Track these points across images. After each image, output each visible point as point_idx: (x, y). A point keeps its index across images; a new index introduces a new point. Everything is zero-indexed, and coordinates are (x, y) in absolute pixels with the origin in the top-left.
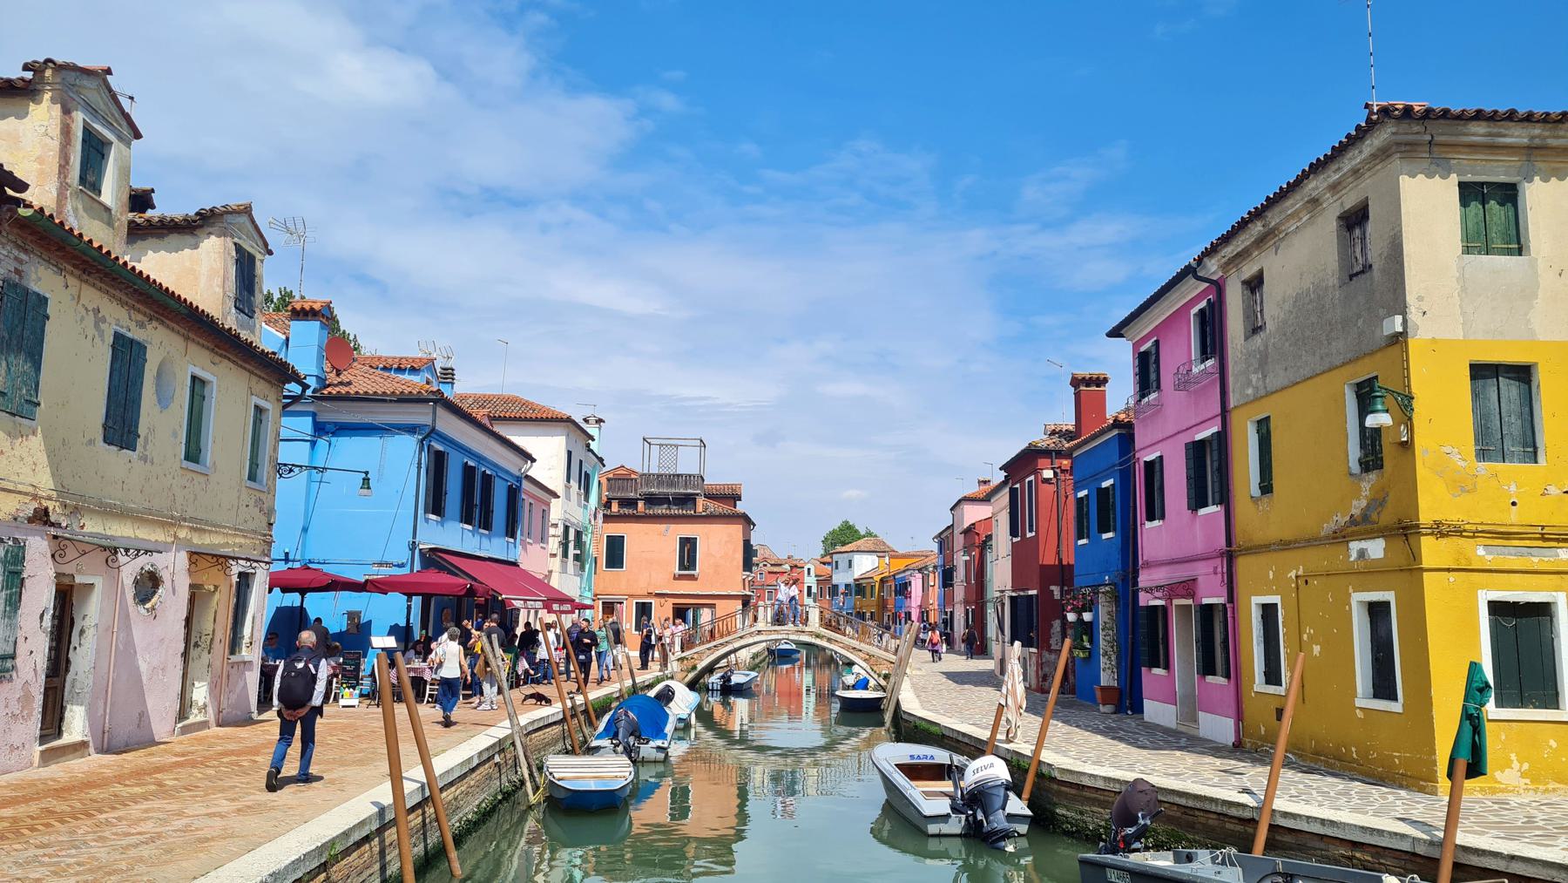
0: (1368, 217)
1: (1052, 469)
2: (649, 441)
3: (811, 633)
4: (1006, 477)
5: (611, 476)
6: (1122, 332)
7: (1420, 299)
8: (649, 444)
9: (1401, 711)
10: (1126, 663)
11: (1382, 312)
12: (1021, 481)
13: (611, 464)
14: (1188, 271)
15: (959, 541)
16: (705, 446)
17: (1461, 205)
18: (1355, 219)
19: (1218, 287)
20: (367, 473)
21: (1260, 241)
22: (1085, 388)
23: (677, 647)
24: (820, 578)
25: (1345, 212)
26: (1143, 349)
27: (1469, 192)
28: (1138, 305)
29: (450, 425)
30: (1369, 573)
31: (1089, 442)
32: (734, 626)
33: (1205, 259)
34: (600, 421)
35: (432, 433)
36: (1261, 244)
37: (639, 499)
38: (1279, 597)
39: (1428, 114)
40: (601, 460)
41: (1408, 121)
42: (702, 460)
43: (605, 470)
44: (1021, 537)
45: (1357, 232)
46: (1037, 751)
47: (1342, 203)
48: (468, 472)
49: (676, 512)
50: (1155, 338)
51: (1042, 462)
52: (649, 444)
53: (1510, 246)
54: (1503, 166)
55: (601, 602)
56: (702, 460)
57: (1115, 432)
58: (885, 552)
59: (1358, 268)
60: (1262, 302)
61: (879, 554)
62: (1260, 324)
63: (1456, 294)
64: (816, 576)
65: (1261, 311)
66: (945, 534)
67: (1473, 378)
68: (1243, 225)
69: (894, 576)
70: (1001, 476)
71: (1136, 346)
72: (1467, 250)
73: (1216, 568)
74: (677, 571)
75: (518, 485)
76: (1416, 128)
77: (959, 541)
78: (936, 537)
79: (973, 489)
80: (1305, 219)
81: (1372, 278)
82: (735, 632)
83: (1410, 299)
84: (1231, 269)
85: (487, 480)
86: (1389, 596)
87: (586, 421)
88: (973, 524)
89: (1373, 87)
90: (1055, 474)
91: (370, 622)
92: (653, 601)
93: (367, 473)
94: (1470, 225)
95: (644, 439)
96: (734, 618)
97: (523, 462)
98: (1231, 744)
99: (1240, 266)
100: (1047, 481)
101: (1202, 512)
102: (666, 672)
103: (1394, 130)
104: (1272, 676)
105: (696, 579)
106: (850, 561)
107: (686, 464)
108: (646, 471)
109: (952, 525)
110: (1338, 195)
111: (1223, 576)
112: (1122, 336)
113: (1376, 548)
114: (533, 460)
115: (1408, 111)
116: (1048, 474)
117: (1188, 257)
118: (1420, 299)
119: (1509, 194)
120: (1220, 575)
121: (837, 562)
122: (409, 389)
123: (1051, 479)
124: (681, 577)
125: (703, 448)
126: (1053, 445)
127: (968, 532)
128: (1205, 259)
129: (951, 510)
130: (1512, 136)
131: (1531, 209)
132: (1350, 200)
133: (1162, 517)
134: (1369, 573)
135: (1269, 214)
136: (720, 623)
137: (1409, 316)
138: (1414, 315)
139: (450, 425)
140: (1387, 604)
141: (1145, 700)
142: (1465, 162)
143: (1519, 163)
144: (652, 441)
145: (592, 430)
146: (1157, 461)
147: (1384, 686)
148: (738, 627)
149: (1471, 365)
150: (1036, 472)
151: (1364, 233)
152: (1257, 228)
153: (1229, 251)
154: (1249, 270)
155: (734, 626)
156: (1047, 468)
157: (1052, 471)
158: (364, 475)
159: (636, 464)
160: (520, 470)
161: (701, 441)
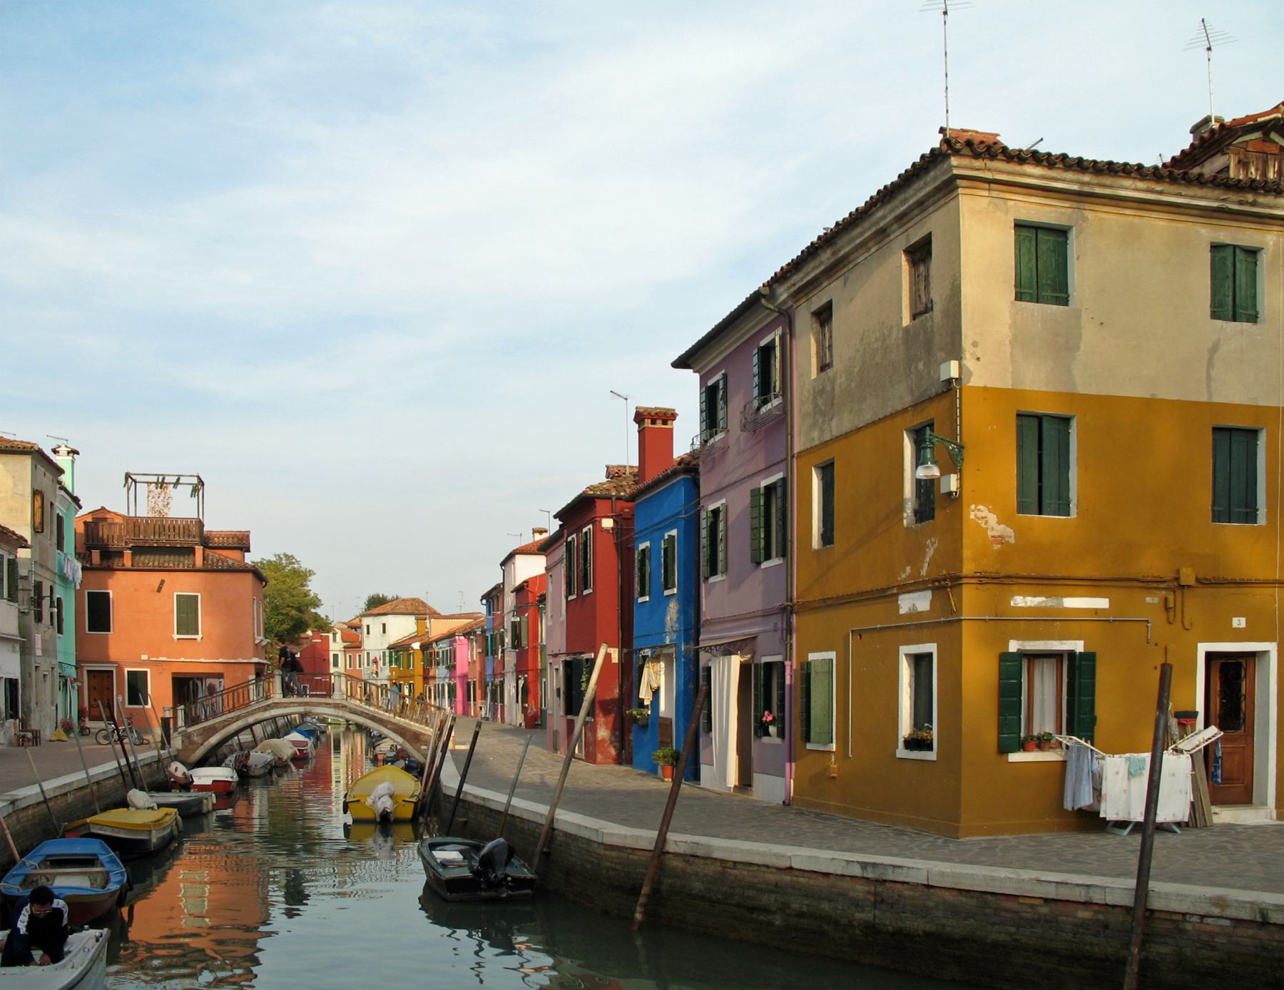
0: (931, 254)
2: (133, 477)
3: (336, 706)
4: (560, 526)
5: (89, 519)
6: (689, 362)
7: (975, 344)
8: (136, 482)
9: (935, 759)
10: (319, 704)
11: (941, 355)
12: (578, 530)
13: (89, 505)
15: (510, 600)
16: (203, 485)
18: (920, 253)
21: (830, 271)
22: (650, 426)
23: (181, 722)
25: (911, 246)
26: (710, 383)
30: (916, 627)
32: (246, 697)
36: (831, 274)
38: (834, 653)
40: (76, 500)
42: (200, 506)
43: (81, 513)
44: (577, 595)
45: (922, 268)
46: (1142, 890)
47: (908, 236)
50: (723, 372)
52: (136, 482)
53: (1059, 295)
54: (1056, 212)
55: (337, 697)
58: (425, 614)
59: (921, 308)
60: (831, 337)
62: (828, 361)
63: (1007, 342)
65: (830, 346)
70: (555, 526)
72: (1019, 297)
73: (776, 624)
77: (510, 600)
78: (483, 597)
79: (529, 539)
80: (873, 250)
81: (932, 318)
82: (248, 705)
83: (966, 343)
84: (801, 298)
86: (931, 648)
87: (55, 451)
88: (525, 582)
91: (555, 517)
92: (148, 670)
94: (1025, 274)
96: (246, 689)
98: (781, 803)
99: (810, 296)
101: (765, 565)
102: (171, 750)
107: (181, 507)
108: (132, 514)
109: (503, 583)
110: (905, 228)
111: (782, 633)
113: (917, 603)
120: (780, 632)
121: (368, 627)
127: (520, 590)
129: (502, 564)
131: (1078, 259)
132: (916, 235)
134: (916, 627)
135: (840, 243)
136: (231, 694)
137: (964, 362)
138: (969, 362)
140: (930, 655)
141: (702, 766)
142: (1021, 204)
143: (1069, 211)
144: (138, 478)
145: (62, 460)
148: (251, 699)
151: (928, 270)
152: (826, 257)
153: (800, 279)
154: (818, 301)
155: (246, 697)
159: (117, 504)
161: (198, 477)
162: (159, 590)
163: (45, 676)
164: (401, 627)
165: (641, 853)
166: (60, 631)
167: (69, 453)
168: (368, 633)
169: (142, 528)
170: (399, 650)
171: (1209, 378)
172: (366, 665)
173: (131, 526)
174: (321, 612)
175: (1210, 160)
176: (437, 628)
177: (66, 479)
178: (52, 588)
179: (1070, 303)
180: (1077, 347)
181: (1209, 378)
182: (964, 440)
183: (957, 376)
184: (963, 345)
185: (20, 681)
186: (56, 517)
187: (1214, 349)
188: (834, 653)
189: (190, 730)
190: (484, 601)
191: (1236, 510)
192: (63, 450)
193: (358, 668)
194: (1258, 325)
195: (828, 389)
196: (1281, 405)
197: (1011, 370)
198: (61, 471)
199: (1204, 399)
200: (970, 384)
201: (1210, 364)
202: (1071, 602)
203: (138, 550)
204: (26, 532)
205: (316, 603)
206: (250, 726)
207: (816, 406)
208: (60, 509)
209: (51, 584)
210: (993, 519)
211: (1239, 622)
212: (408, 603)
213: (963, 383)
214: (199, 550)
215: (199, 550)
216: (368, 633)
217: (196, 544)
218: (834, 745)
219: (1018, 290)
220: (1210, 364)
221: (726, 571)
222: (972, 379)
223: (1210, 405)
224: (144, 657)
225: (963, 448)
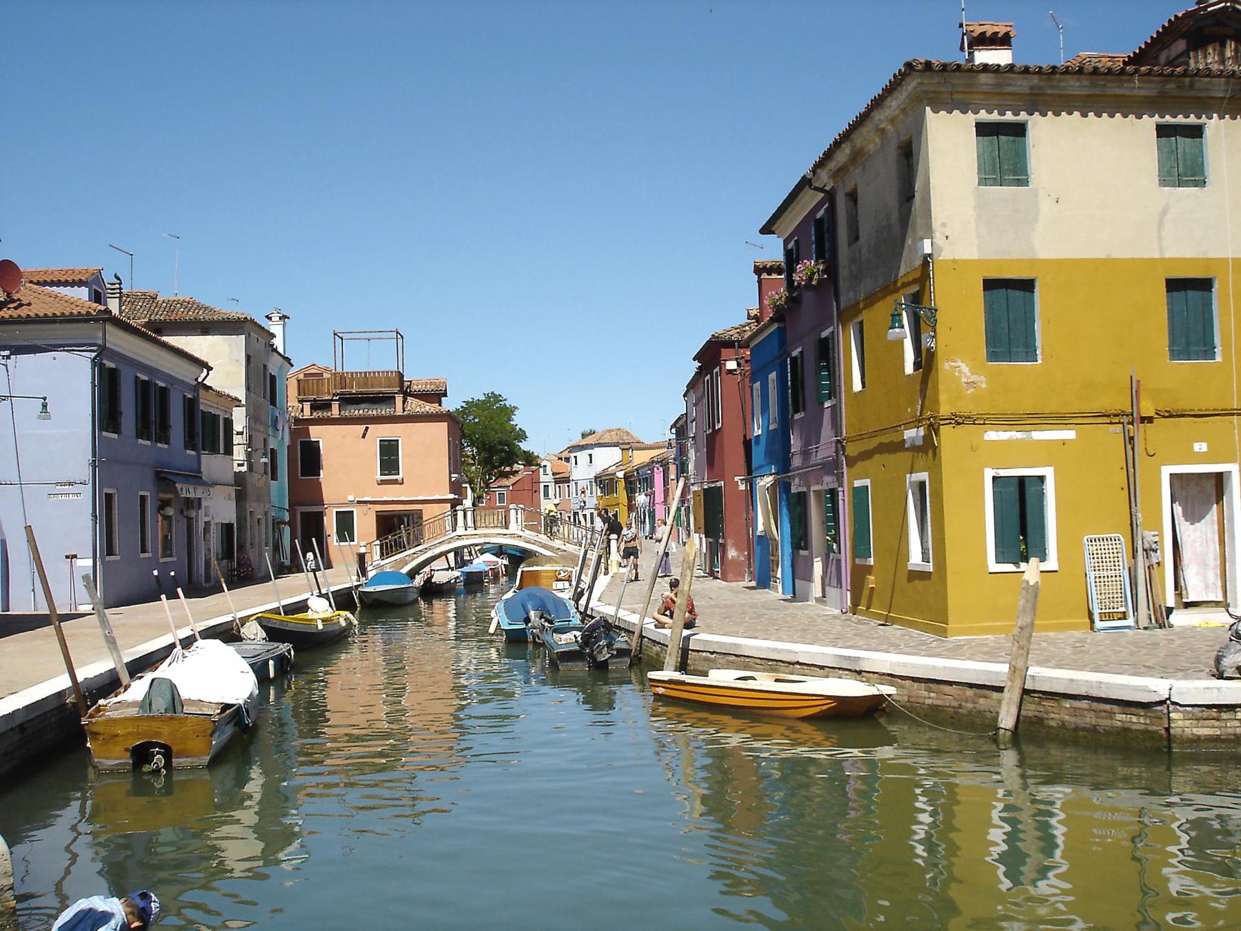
1: (736, 359)
3: (512, 536)
5: (301, 376)
6: (773, 229)
8: (342, 339)
14: (804, 183)
17: (5, 540)
19: (830, 196)
20: (45, 399)
22: (767, 277)
23: (377, 556)
24: (557, 476)
27: (983, 129)
28: (782, 201)
29: (118, 340)
31: (763, 330)
33: (818, 171)
34: (283, 318)
35: (103, 351)
37: (332, 400)
38: (869, 480)
39: (944, 67)
40: (288, 360)
41: (929, 73)
42: (400, 352)
43: (293, 370)
48: (144, 389)
49: (375, 413)
51: (725, 352)
56: (400, 352)
57: (775, 326)
61: (622, 447)
64: (554, 474)
66: (681, 423)
67: (985, 289)
68: (837, 144)
69: (637, 470)
71: (786, 242)
72: (983, 182)
74: (380, 477)
75: (196, 395)
76: (936, 80)
85: (164, 393)
89: (963, 10)
90: (739, 365)
91: (694, 359)
93: (45, 399)
95: (335, 334)
97: (198, 371)
100: (730, 372)
103: (919, 80)
104: (143, 498)
105: (402, 483)
106: (590, 455)
108: (339, 370)
112: (773, 233)
114: (209, 369)
115: (928, 65)
116: (731, 365)
117: (805, 169)
118: (944, 225)
119: (1019, 130)
122: (78, 309)
123: (735, 370)
124: (383, 482)
125: (400, 341)
126: (736, 335)
128: (818, 171)
129: (684, 396)
130: (1015, 85)
133: (804, 409)
137: (934, 240)
139: (118, 340)
144: (344, 336)
146: (799, 356)
147: (109, 497)
149: (984, 280)
150: (722, 366)
156: (731, 360)
157: (735, 362)
158: (42, 400)
160: (197, 379)
161: (397, 333)
162: (364, 437)
163: (259, 520)
164: (607, 459)
165: (946, 689)
166: (274, 477)
167: (280, 318)
168: (576, 464)
169: (348, 381)
170: (605, 482)
171: (1160, 238)
172: (574, 496)
173: (338, 379)
174: (524, 446)
175: (1174, 44)
176: (641, 457)
177: (278, 342)
178: (265, 440)
179: (1030, 184)
180: (1035, 220)
181: (1160, 238)
182: (937, 304)
183: (930, 252)
184: (933, 226)
185: (927, 484)
186: (268, 376)
187: (1164, 212)
188: (869, 480)
189: (383, 563)
190: (674, 431)
191: (1194, 348)
192: (275, 318)
193: (567, 497)
194: (1208, 188)
195: (858, 256)
196: (1230, 256)
197: (977, 243)
198: (273, 336)
199: (1156, 255)
200: (941, 258)
201: (1161, 225)
202: (1038, 435)
203: (348, 400)
204: (241, 394)
205: (522, 435)
206: (445, 554)
207: (851, 272)
208: (273, 370)
209: (264, 436)
210: (965, 369)
211: (1200, 447)
212: (614, 433)
213: (934, 258)
214: (399, 399)
215: (399, 399)
216: (576, 464)
217: (396, 393)
218: (872, 559)
219: (983, 176)
220: (1161, 225)
221: (804, 409)
222: (942, 254)
223: (1162, 260)
224: (351, 498)
225: (936, 310)
